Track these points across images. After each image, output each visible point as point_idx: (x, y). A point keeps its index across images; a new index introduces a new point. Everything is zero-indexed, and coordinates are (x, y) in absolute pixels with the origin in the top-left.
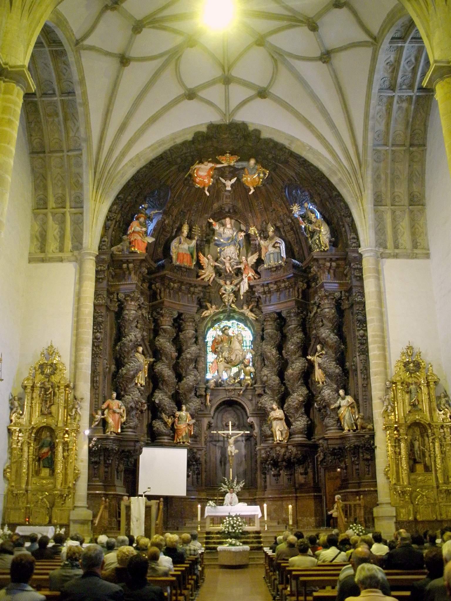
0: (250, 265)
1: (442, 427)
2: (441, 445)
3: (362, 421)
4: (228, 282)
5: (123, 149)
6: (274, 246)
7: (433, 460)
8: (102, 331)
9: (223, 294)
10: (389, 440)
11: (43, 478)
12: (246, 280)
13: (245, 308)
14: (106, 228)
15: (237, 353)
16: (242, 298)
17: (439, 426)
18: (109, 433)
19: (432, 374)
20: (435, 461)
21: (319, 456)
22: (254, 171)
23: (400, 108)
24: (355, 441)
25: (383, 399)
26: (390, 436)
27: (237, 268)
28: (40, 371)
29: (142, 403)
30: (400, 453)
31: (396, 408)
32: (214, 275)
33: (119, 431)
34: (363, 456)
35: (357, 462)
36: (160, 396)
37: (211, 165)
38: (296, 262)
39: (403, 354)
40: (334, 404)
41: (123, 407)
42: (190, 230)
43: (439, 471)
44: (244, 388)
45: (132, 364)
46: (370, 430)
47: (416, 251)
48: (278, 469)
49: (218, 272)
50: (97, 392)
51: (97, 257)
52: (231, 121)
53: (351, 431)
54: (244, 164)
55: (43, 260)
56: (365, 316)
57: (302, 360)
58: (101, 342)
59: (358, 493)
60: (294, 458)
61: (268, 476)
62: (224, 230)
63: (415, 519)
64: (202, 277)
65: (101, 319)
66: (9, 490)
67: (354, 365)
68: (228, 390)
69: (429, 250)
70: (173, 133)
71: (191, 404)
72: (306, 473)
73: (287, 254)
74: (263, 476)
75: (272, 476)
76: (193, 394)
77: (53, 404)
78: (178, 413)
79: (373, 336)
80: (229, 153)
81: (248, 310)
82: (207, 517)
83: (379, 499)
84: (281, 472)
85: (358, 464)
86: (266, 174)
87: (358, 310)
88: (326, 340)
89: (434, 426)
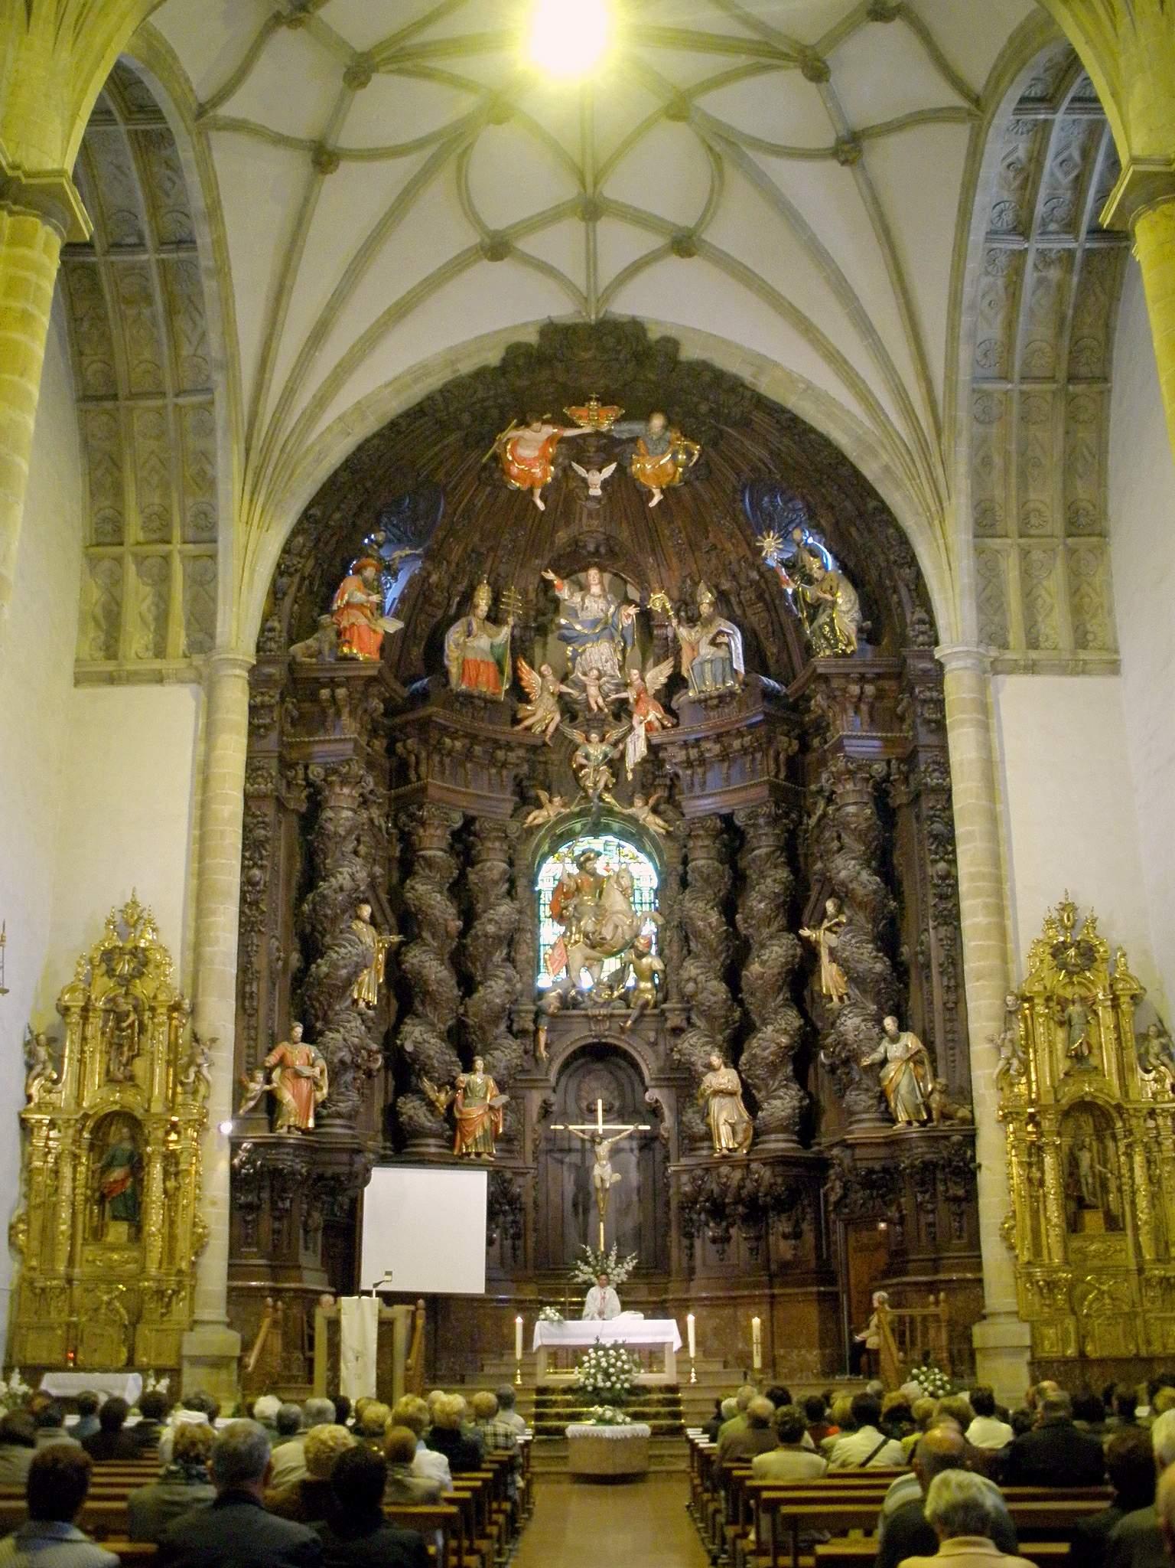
0: (651, 692)
1: (1152, 1114)
2: (1149, 1162)
3: (944, 1099)
4: (594, 737)
5: (320, 389)
6: (713, 643)
7: (1127, 1199)
8: (265, 862)
9: (582, 767)
10: (1013, 1147)
11: (113, 1248)
12: (640, 730)
13: (638, 802)
14: (276, 594)
15: (618, 922)
16: (630, 776)
17: (1145, 1112)
18: (285, 1129)
19: (1127, 977)
20: (1133, 1203)
21: (832, 1188)
22: (663, 445)
23: (1041, 282)
24: (925, 1149)
25: (999, 1042)
26: (1016, 1138)
27: (617, 699)
28: (104, 967)
29: (370, 1052)
30: (1042, 1183)
31: (1032, 1064)
32: (558, 718)
33: (311, 1123)
34: (947, 1190)
35: (930, 1207)
36: (417, 1033)
37: (549, 430)
38: (772, 683)
39: (1050, 923)
40: (870, 1054)
41: (321, 1063)
42: (496, 600)
43: (1145, 1229)
44: (635, 1013)
45: (343, 951)
46: (963, 1121)
47: (1083, 655)
48: (724, 1224)
49: (569, 709)
50: (253, 1022)
51: (253, 670)
52: (601, 315)
53: (916, 1124)
54: (637, 427)
55: (111, 680)
56: (950, 823)
57: (788, 939)
58: (263, 892)
59: (932, 1287)
60: (766, 1195)
61: (698, 1243)
62: (583, 600)
63: (1082, 1354)
64: (527, 723)
65: (263, 832)
66: (23, 1278)
67: (922, 953)
68: (595, 1016)
69: (1116, 652)
70: (451, 348)
71: (497, 1053)
72: (797, 1235)
73: (747, 661)
74: (686, 1242)
75: (708, 1242)
76: (503, 1027)
77: (138, 1055)
78: (463, 1078)
79: (973, 877)
80: (597, 400)
81: (647, 808)
82: (539, 1348)
83: (987, 1302)
84: (733, 1231)
85: (933, 1211)
86: (692, 454)
87: (932, 808)
88: (851, 886)
89: (1131, 1112)
